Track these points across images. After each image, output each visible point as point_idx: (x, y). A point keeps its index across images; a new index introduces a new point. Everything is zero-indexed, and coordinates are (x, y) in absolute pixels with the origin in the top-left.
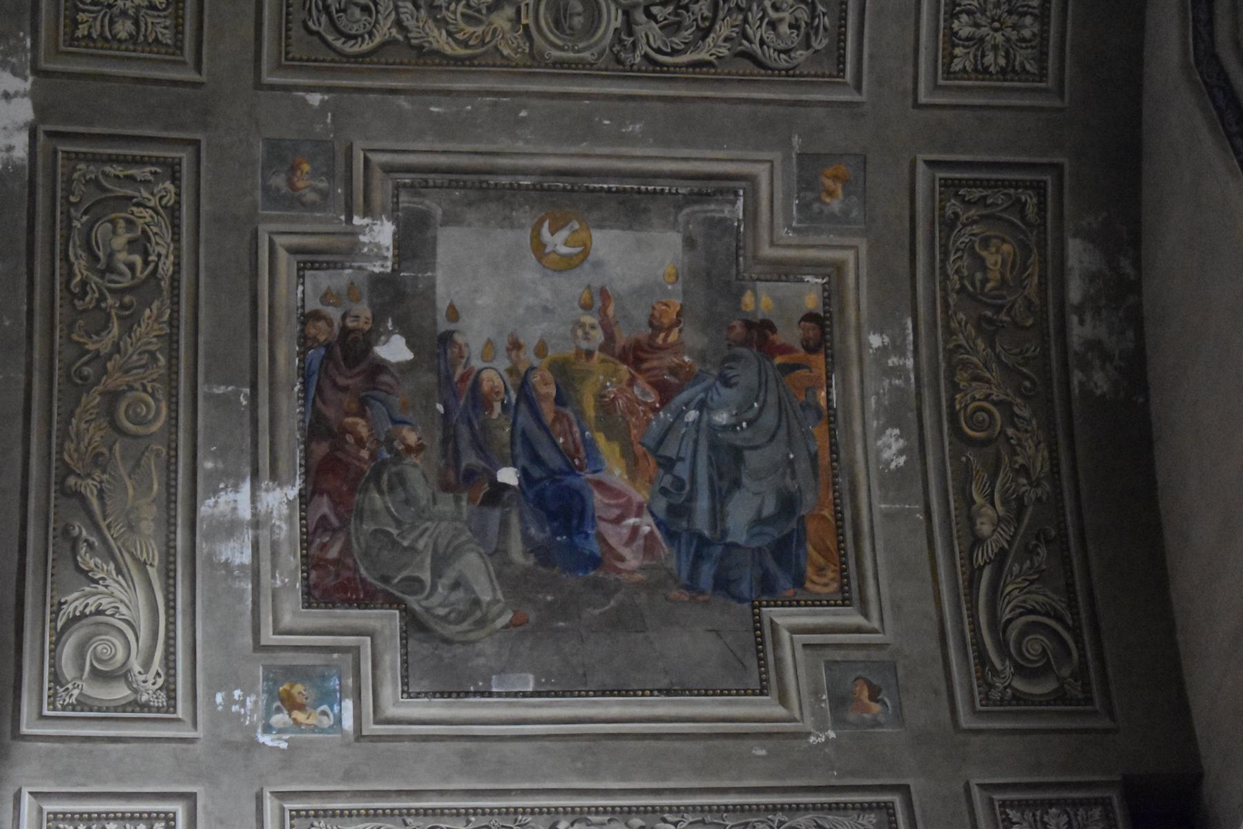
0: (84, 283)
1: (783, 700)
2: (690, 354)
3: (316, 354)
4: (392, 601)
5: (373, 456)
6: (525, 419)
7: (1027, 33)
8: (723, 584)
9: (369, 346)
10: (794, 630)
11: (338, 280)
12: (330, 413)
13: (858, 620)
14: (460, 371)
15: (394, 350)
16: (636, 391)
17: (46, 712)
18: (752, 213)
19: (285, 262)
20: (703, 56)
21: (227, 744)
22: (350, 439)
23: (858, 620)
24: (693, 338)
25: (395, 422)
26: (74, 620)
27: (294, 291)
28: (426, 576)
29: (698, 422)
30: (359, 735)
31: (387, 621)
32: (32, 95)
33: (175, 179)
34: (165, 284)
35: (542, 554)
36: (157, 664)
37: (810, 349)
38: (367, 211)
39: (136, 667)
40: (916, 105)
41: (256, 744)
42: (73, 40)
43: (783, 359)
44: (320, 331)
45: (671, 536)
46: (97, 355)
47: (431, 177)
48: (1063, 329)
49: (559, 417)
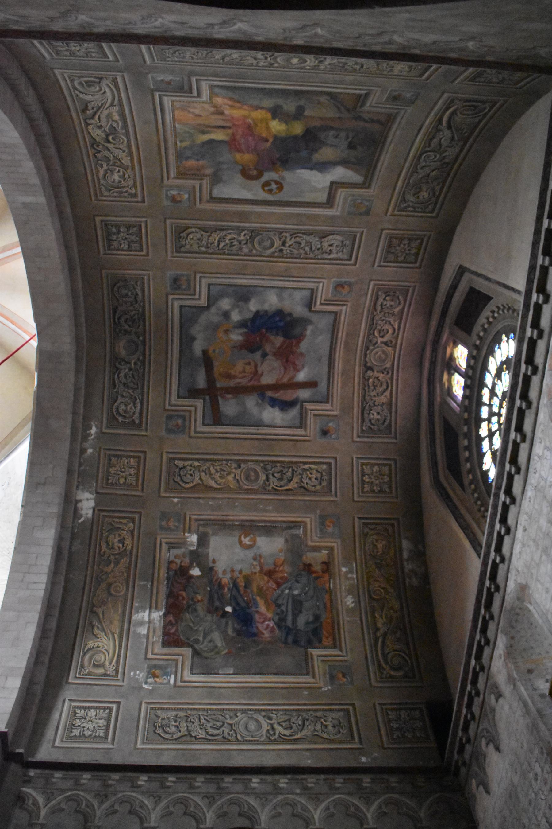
0: (105, 552)
1: (314, 677)
2: (287, 573)
3: (172, 573)
4: (189, 646)
5: (187, 603)
6: (235, 592)
7: (386, 481)
8: (296, 642)
9: (188, 572)
10: (318, 656)
11: (180, 552)
12: (175, 590)
13: (340, 653)
14: (215, 578)
15: (196, 572)
16: (270, 584)
17: (77, 676)
18: (305, 531)
19: (165, 547)
20: (289, 487)
21: (133, 687)
22: (181, 598)
23: (340, 653)
24: (287, 569)
25: (194, 592)
26: (90, 649)
27: (166, 554)
28: (201, 639)
29: (288, 594)
30: (175, 685)
31: (188, 652)
32: (95, 499)
33: (134, 522)
34: (128, 553)
35: (239, 633)
36: (114, 663)
37: (323, 572)
38: (189, 532)
39: (107, 663)
40: (354, 501)
41: (142, 688)
42: (107, 484)
43: (314, 575)
44: (174, 567)
45: (279, 627)
46: (106, 573)
47: (209, 522)
48: (402, 568)
49: (245, 592)
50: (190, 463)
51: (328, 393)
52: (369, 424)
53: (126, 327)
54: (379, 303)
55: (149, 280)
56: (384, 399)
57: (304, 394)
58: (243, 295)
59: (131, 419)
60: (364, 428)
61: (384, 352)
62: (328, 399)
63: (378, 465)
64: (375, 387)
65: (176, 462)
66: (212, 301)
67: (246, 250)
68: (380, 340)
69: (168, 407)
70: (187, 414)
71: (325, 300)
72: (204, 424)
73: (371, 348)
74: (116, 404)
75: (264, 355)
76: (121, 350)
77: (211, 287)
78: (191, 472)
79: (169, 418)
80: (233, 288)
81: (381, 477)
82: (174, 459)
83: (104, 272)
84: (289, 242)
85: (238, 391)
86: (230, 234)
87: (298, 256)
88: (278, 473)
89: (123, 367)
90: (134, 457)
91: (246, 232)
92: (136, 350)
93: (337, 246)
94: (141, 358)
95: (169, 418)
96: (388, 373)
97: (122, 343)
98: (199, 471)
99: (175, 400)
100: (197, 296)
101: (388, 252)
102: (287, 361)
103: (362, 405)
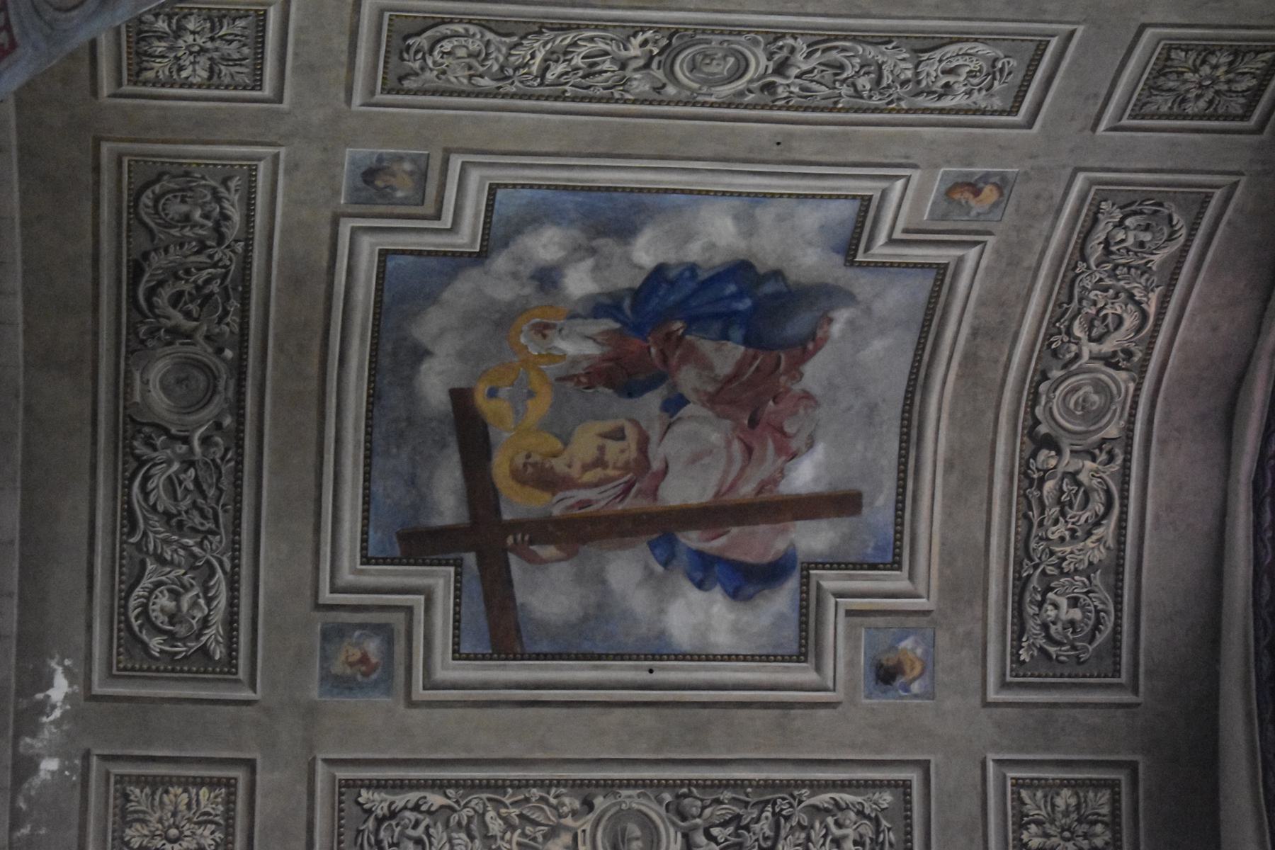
50: (413, 796)
51: (899, 533)
52: (1041, 641)
53: (178, 318)
54: (1100, 235)
55: (275, 173)
56: (1094, 550)
57: (813, 538)
58: (612, 218)
59: (194, 645)
60: (1024, 656)
61: (1100, 387)
62: (898, 555)
63: (1074, 785)
64: (1064, 507)
65: (365, 795)
66: (494, 238)
67: (640, 85)
68: (1088, 349)
69: (327, 596)
70: (398, 619)
71: (906, 231)
72: (457, 654)
73: (1056, 374)
74: (138, 591)
75: (674, 404)
76: (154, 390)
77: (500, 194)
78: (420, 832)
79: (333, 635)
80: (580, 198)
81: (1085, 827)
82: (354, 785)
83: (105, 147)
84: (801, 63)
85: (579, 533)
86: (591, 39)
87: (829, 103)
88: (724, 824)
89: (160, 456)
90: (213, 784)
91: (649, 34)
92: (212, 390)
93: (971, 74)
94: (228, 421)
95: (333, 635)
96: (1111, 458)
97: (157, 370)
98: (447, 825)
99: (355, 572)
100: (447, 222)
101: (1153, 88)
102: (753, 423)
103: (1018, 571)
